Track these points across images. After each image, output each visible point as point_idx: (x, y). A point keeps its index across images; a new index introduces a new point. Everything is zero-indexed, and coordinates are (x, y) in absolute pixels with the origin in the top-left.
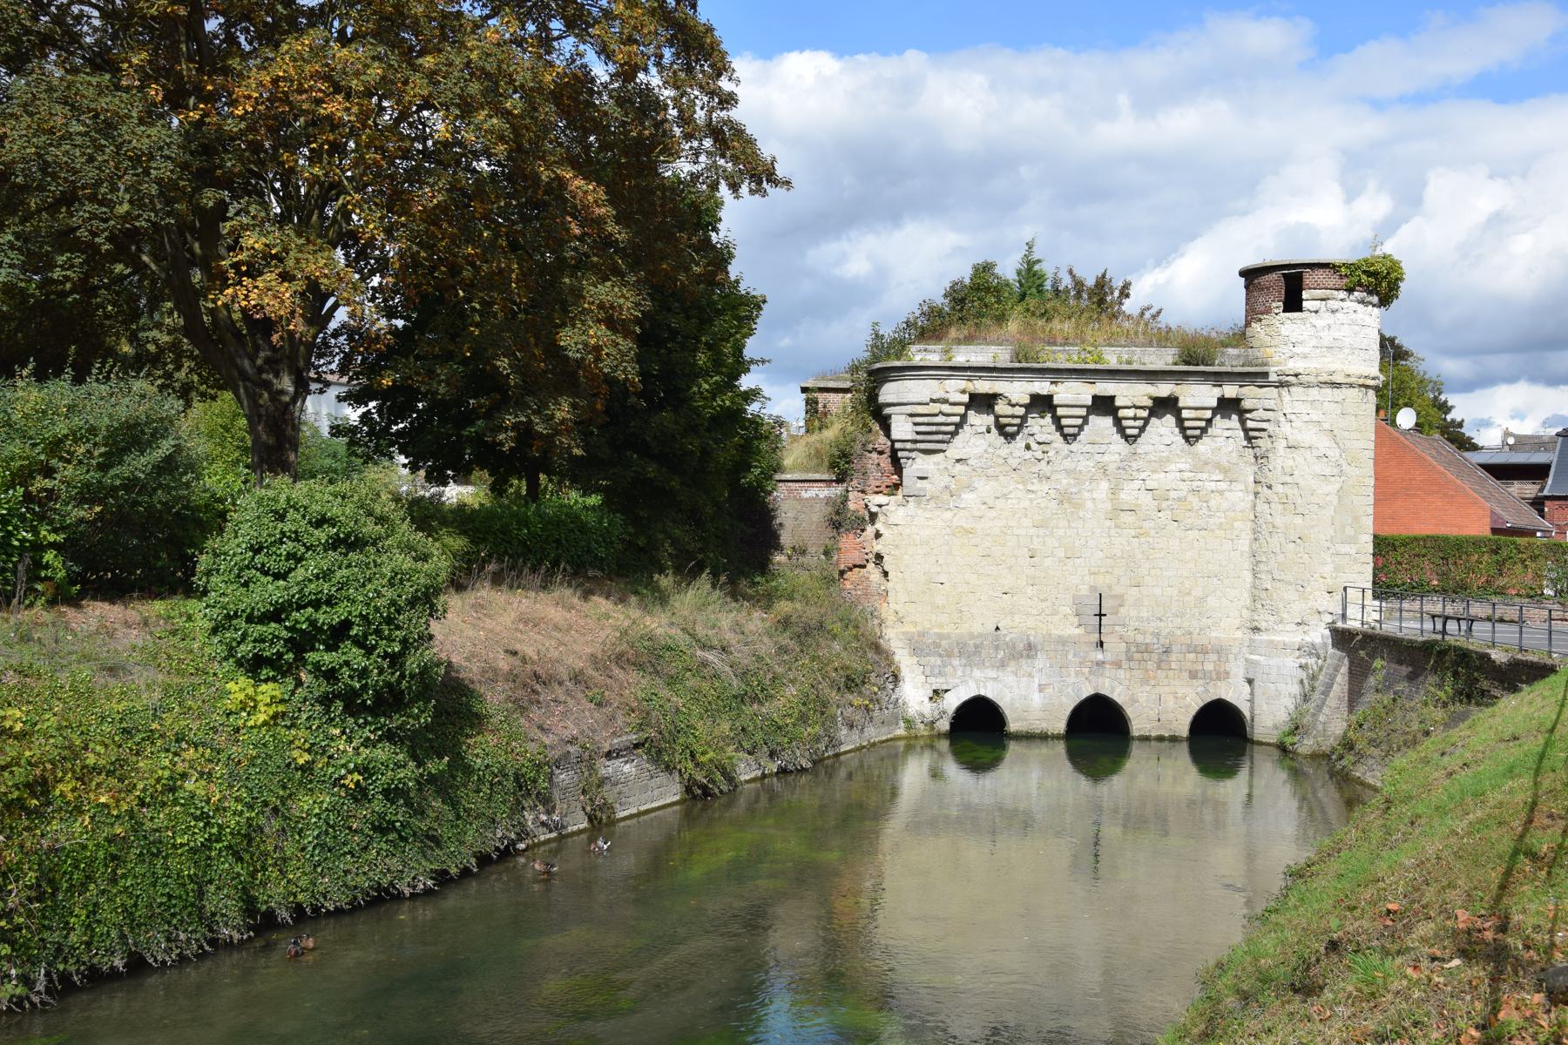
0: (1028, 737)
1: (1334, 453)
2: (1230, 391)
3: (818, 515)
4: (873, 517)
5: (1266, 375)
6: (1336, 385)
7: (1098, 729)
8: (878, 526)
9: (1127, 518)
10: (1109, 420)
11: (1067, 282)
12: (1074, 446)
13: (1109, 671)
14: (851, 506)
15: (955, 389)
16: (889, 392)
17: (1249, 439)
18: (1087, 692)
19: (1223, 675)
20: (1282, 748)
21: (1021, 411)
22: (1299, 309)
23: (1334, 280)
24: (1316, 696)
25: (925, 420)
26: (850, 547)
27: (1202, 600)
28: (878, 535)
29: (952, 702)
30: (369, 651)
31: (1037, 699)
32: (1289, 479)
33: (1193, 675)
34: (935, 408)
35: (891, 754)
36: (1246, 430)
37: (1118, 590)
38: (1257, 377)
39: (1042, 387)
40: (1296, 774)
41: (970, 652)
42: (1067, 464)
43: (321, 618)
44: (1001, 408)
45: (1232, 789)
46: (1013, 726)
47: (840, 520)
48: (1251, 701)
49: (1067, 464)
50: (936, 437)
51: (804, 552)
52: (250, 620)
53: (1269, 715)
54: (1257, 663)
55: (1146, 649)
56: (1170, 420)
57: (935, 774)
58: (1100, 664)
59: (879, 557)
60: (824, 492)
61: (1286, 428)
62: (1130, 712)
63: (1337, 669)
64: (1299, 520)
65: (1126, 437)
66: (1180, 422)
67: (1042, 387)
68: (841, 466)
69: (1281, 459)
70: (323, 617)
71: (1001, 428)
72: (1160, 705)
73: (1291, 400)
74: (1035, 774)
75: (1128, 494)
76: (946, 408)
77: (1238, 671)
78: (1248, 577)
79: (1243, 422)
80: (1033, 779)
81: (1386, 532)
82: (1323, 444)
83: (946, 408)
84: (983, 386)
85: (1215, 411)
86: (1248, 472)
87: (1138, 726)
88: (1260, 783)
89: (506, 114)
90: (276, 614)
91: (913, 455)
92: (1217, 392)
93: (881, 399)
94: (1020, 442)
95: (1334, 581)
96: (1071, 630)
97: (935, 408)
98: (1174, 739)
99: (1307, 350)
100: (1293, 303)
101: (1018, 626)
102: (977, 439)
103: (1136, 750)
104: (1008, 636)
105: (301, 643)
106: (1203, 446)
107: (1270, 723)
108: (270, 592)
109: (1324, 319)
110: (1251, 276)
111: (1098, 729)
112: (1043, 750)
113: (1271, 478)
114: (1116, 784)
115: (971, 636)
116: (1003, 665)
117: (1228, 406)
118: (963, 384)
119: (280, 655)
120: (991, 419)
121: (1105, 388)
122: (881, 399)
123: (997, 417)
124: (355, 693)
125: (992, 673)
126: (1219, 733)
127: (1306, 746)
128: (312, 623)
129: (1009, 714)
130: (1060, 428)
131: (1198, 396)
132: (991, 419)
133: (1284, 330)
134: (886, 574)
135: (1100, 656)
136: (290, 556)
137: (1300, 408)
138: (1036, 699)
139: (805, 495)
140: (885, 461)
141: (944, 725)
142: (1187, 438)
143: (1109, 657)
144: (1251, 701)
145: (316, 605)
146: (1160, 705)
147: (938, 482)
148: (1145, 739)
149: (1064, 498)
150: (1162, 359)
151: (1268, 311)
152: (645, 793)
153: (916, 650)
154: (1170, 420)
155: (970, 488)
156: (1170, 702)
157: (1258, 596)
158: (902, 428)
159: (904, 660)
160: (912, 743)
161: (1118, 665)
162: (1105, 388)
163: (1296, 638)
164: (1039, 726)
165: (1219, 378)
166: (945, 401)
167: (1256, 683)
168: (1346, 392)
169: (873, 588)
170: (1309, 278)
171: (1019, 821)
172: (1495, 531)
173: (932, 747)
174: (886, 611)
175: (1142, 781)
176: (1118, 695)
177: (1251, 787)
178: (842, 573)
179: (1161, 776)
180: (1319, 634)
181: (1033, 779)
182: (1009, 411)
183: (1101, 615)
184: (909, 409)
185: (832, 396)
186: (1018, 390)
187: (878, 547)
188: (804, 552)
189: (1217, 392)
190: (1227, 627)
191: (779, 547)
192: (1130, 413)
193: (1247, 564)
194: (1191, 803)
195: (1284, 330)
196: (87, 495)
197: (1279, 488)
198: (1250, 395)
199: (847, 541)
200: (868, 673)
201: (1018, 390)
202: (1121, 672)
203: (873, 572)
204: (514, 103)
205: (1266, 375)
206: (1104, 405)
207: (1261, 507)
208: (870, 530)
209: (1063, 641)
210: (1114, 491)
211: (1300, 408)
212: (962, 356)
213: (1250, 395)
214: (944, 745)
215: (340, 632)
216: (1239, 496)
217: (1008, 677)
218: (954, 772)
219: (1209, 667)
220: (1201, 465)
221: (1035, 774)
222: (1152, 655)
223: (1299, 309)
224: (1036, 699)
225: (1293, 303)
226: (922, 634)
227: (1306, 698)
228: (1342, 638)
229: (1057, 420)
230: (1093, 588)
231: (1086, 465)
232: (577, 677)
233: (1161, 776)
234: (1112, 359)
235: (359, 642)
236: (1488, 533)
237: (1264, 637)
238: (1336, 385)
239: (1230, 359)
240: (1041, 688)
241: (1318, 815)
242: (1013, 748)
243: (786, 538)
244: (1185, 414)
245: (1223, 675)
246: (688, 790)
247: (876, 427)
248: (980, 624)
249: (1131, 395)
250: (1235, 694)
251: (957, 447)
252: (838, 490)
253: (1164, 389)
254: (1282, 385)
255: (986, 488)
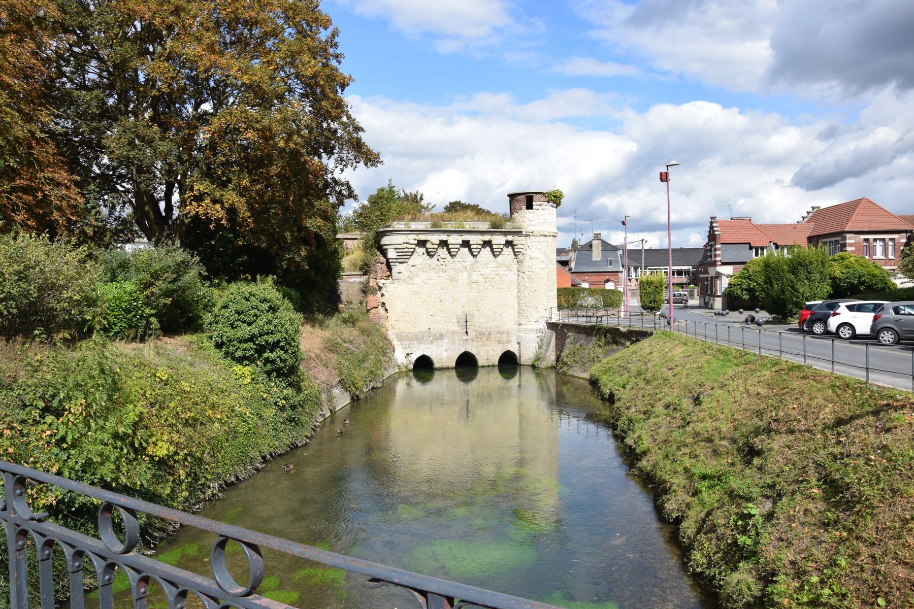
0: (442, 369)
1: (545, 260)
2: (510, 238)
3: (357, 288)
4: (380, 288)
5: (521, 232)
6: (545, 236)
7: (467, 365)
8: (383, 291)
9: (475, 285)
10: (467, 249)
11: (402, 195)
12: (455, 259)
14: (371, 284)
15: (412, 238)
16: (385, 240)
17: (515, 255)
19: (509, 342)
20: (533, 367)
21: (436, 246)
22: (532, 208)
23: (543, 198)
24: (544, 347)
26: (372, 300)
27: (501, 315)
28: (382, 295)
29: (414, 358)
30: (286, 351)
31: (445, 355)
33: (499, 342)
34: (405, 246)
35: (394, 379)
36: (514, 252)
37: (472, 312)
38: (519, 233)
39: (444, 237)
40: (538, 375)
41: (419, 338)
42: (452, 266)
43: (271, 340)
44: (428, 245)
45: (514, 382)
46: (436, 365)
47: (365, 290)
48: (520, 350)
49: (452, 266)
50: (404, 257)
51: (351, 303)
52: (240, 342)
53: (527, 355)
54: (521, 337)
55: (482, 334)
56: (488, 249)
57: (408, 385)
58: (467, 340)
59: (383, 304)
60: (358, 279)
61: (529, 251)
62: (478, 357)
63: (551, 337)
65: (473, 256)
66: (492, 249)
67: (444, 237)
68: (365, 269)
69: (527, 262)
70: (271, 339)
71: (428, 253)
72: (488, 354)
73: (530, 241)
74: (445, 382)
75: (475, 276)
76: (409, 246)
77: (514, 340)
78: (517, 305)
79: (513, 249)
80: (444, 384)
81: (561, 287)
82: (542, 256)
83: (409, 246)
84: (422, 237)
85: (439, 245)
86: (515, 267)
87: (481, 362)
88: (524, 378)
89: (303, 137)
90: (251, 339)
92: (505, 239)
93: (382, 243)
94: (435, 258)
95: (545, 307)
96: (456, 328)
97: (405, 246)
98: (493, 366)
100: (530, 206)
101: (437, 327)
103: (480, 371)
104: (433, 331)
105: (260, 350)
106: (500, 258)
108: (245, 331)
109: (541, 212)
110: (512, 197)
111: (467, 365)
112: (447, 373)
113: (524, 269)
114: (473, 384)
115: (420, 332)
116: (432, 343)
117: (509, 244)
118: (415, 237)
119: (252, 355)
120: (424, 250)
121: (466, 237)
122: (382, 243)
123: (427, 249)
124: (281, 368)
125: (428, 346)
126: (509, 363)
127: (544, 365)
128: (266, 342)
129: (435, 361)
130: (450, 252)
131: (498, 240)
132: (424, 250)
133: (527, 216)
134: (386, 310)
135: (466, 337)
136: (255, 315)
137: (533, 244)
138: (444, 355)
139: (350, 281)
140: (384, 267)
141: (411, 367)
142: (494, 255)
143: (469, 337)
144: (520, 350)
145: (267, 334)
146: (488, 354)
147: (406, 274)
148: (483, 367)
149: (452, 279)
150: (485, 226)
151: (521, 209)
152: (342, 400)
153: (399, 339)
154: (488, 249)
155: (417, 276)
156: (491, 353)
157: (520, 312)
158: (392, 254)
159: (395, 343)
160: (400, 375)
161: (473, 340)
162: (466, 237)
163: (536, 326)
164: (445, 365)
165: (505, 233)
167: (522, 344)
168: (548, 238)
169: (382, 316)
170: (535, 197)
171: (437, 401)
172: (573, 285)
173: (407, 376)
174: (388, 325)
175: (482, 384)
176: (473, 351)
177: (520, 381)
178: (368, 311)
179: (489, 380)
180: (543, 325)
181: (444, 384)
182: (432, 246)
185: (348, 241)
186: (435, 239)
187: (383, 300)
188: (351, 303)
189: (505, 239)
190: (509, 324)
191: (341, 302)
192: (475, 246)
193: (516, 301)
194: (500, 389)
195: (527, 216)
196: (167, 294)
197: (527, 273)
198: (516, 240)
199: (370, 298)
200: (386, 349)
201: (435, 239)
203: (381, 310)
204: (305, 132)
205: (521, 232)
206: (466, 244)
207: (520, 279)
208: (379, 293)
209: (453, 332)
210: (470, 276)
211: (533, 244)
212: (414, 226)
213: (516, 240)
214: (411, 374)
215: (275, 346)
216: (513, 276)
217: (434, 347)
218: (415, 383)
219: (504, 339)
220: (500, 265)
221: (445, 382)
222: (484, 336)
223: (532, 208)
224: (444, 355)
225: (530, 206)
226: (402, 333)
227: (540, 347)
228: (552, 326)
229: (449, 250)
230: (463, 312)
231: (459, 266)
232: (318, 357)
233: (489, 380)
234: (467, 226)
235: (282, 348)
236: (570, 286)
237: (523, 327)
238: (545, 236)
239: (508, 226)
240: (446, 351)
241: (545, 389)
242: (436, 372)
243: (344, 298)
244: (494, 247)
245: (509, 342)
246: (352, 398)
247: (379, 253)
248: (423, 327)
249: (475, 240)
250: (514, 348)
251: (412, 261)
252: (364, 278)
253: (487, 238)
254: (527, 236)
255: (423, 276)
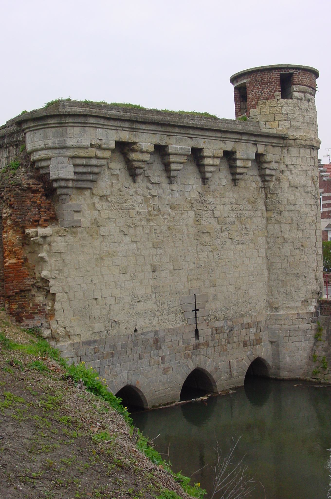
9: (206, 238)
13: (203, 350)
18: (192, 367)
25: (84, 162)
32: (293, 208)
34: (93, 152)
64: (300, 234)
76: (100, 154)
83: (100, 154)
91: (69, 191)
99: (298, 124)
102: (112, 179)
107: (82, 332)
166: (100, 147)
183: (196, 310)
184: (71, 153)
198: (272, 155)
202: (209, 349)
225: (286, 93)
